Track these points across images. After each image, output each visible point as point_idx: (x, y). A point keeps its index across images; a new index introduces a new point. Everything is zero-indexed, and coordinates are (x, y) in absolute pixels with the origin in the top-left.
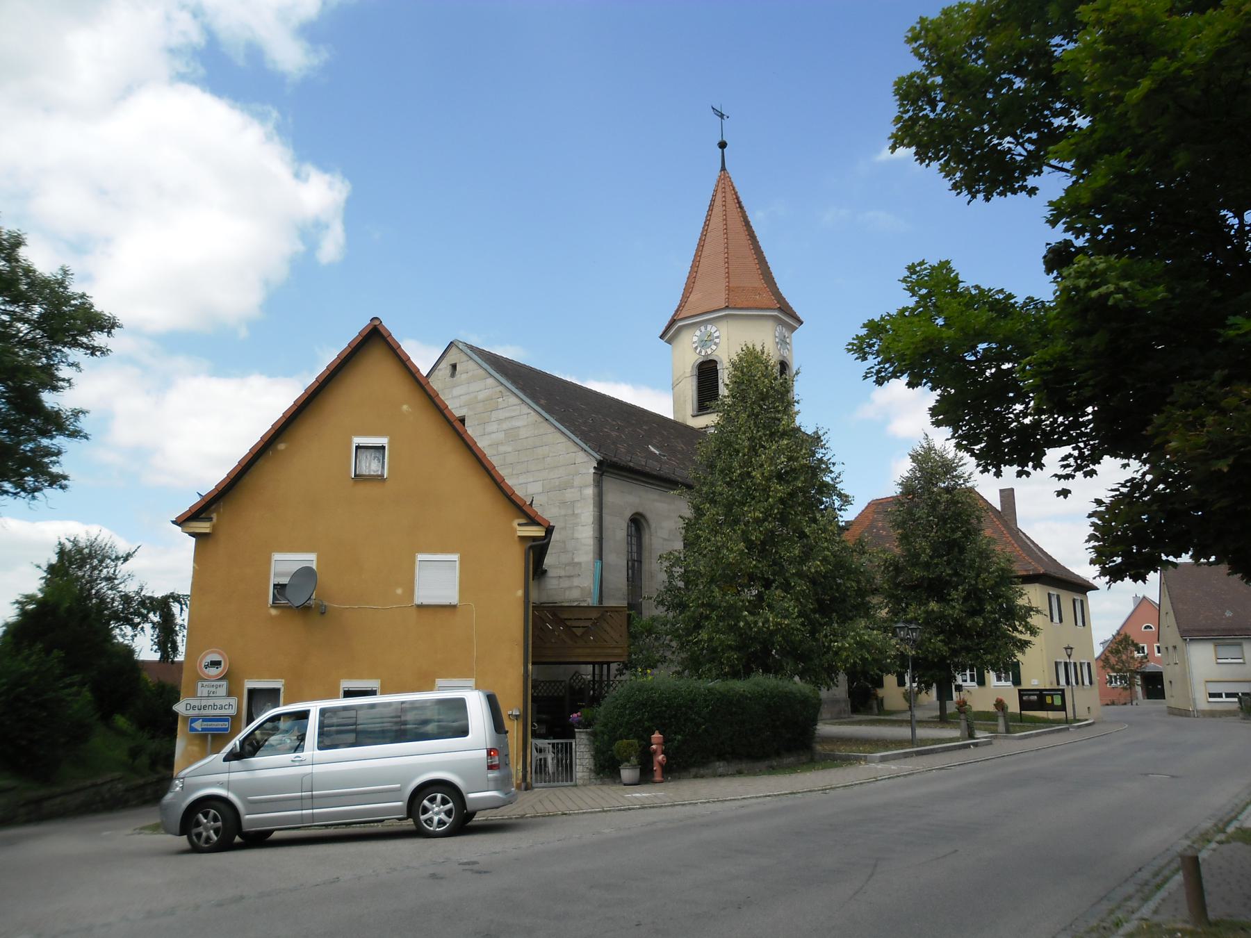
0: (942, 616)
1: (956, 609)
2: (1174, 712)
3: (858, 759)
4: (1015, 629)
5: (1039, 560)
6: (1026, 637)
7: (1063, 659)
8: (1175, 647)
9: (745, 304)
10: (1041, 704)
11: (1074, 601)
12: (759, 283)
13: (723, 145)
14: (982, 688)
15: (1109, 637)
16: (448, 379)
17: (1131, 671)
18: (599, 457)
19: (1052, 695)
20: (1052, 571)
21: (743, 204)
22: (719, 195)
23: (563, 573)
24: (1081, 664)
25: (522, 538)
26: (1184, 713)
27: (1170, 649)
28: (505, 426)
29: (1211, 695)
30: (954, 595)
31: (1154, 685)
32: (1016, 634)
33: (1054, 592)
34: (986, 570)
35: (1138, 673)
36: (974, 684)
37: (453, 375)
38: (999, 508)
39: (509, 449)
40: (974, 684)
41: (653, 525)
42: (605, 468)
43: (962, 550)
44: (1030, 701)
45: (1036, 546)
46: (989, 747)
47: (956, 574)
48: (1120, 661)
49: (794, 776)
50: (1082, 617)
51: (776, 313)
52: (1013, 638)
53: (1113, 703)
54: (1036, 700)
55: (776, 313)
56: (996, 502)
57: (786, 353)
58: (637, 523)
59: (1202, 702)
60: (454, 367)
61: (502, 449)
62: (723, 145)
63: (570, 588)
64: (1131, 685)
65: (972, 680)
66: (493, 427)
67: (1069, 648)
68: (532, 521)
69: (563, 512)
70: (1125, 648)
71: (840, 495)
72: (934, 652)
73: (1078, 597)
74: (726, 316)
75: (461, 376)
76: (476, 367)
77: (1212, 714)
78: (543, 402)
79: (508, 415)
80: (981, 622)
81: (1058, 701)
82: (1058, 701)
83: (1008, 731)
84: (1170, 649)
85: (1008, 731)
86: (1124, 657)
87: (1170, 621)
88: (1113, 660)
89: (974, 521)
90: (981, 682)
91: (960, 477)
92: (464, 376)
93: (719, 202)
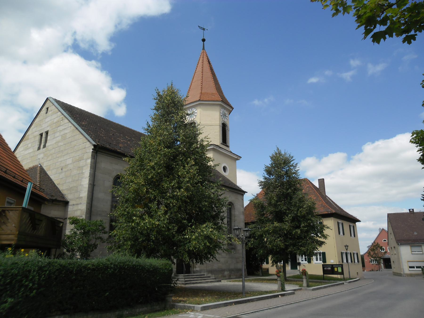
0: (281, 229)
1: (286, 226)
2: (395, 274)
3: (189, 308)
4: (318, 236)
5: (334, 208)
6: (322, 240)
7: (345, 251)
8: (394, 247)
9: (207, 99)
10: (333, 272)
11: (350, 226)
12: (215, 91)
13: (204, 40)
14: (310, 264)
15: (371, 244)
16: (45, 115)
17: (379, 257)
18: (94, 143)
19: (337, 267)
20: (339, 212)
21: (211, 63)
22: (201, 59)
23: (75, 203)
24: (354, 254)
26: (400, 275)
27: (393, 248)
28: (62, 133)
29: (410, 267)
30: (287, 219)
31: (388, 263)
32: (318, 238)
33: (340, 221)
34: (302, 207)
35: (381, 258)
36: (306, 262)
37: (47, 113)
38: (318, 187)
40: (306, 262)
42: (98, 150)
43: (291, 198)
44: (327, 270)
45: (334, 203)
46: (292, 296)
47: (289, 209)
48: (375, 253)
49: (164, 315)
50: (354, 233)
51: (220, 103)
52: (317, 240)
53: (373, 270)
54: (329, 270)
55: (220, 103)
56: (317, 184)
57: (226, 120)
59: (407, 271)
60: (48, 109)
62: (204, 40)
64: (379, 263)
65: (306, 260)
66: (57, 134)
67: (346, 246)
69: (78, 172)
70: (377, 249)
72: (276, 246)
73: (352, 224)
74: (199, 104)
75: (50, 113)
76: (55, 108)
77: (411, 275)
79: (63, 128)
80: (299, 231)
81: (340, 270)
82: (340, 270)
83: (308, 286)
84: (393, 248)
85: (308, 286)
86: (376, 252)
87: (392, 237)
88: (372, 253)
89: (298, 185)
90: (309, 262)
91: (292, 166)
93: (201, 61)
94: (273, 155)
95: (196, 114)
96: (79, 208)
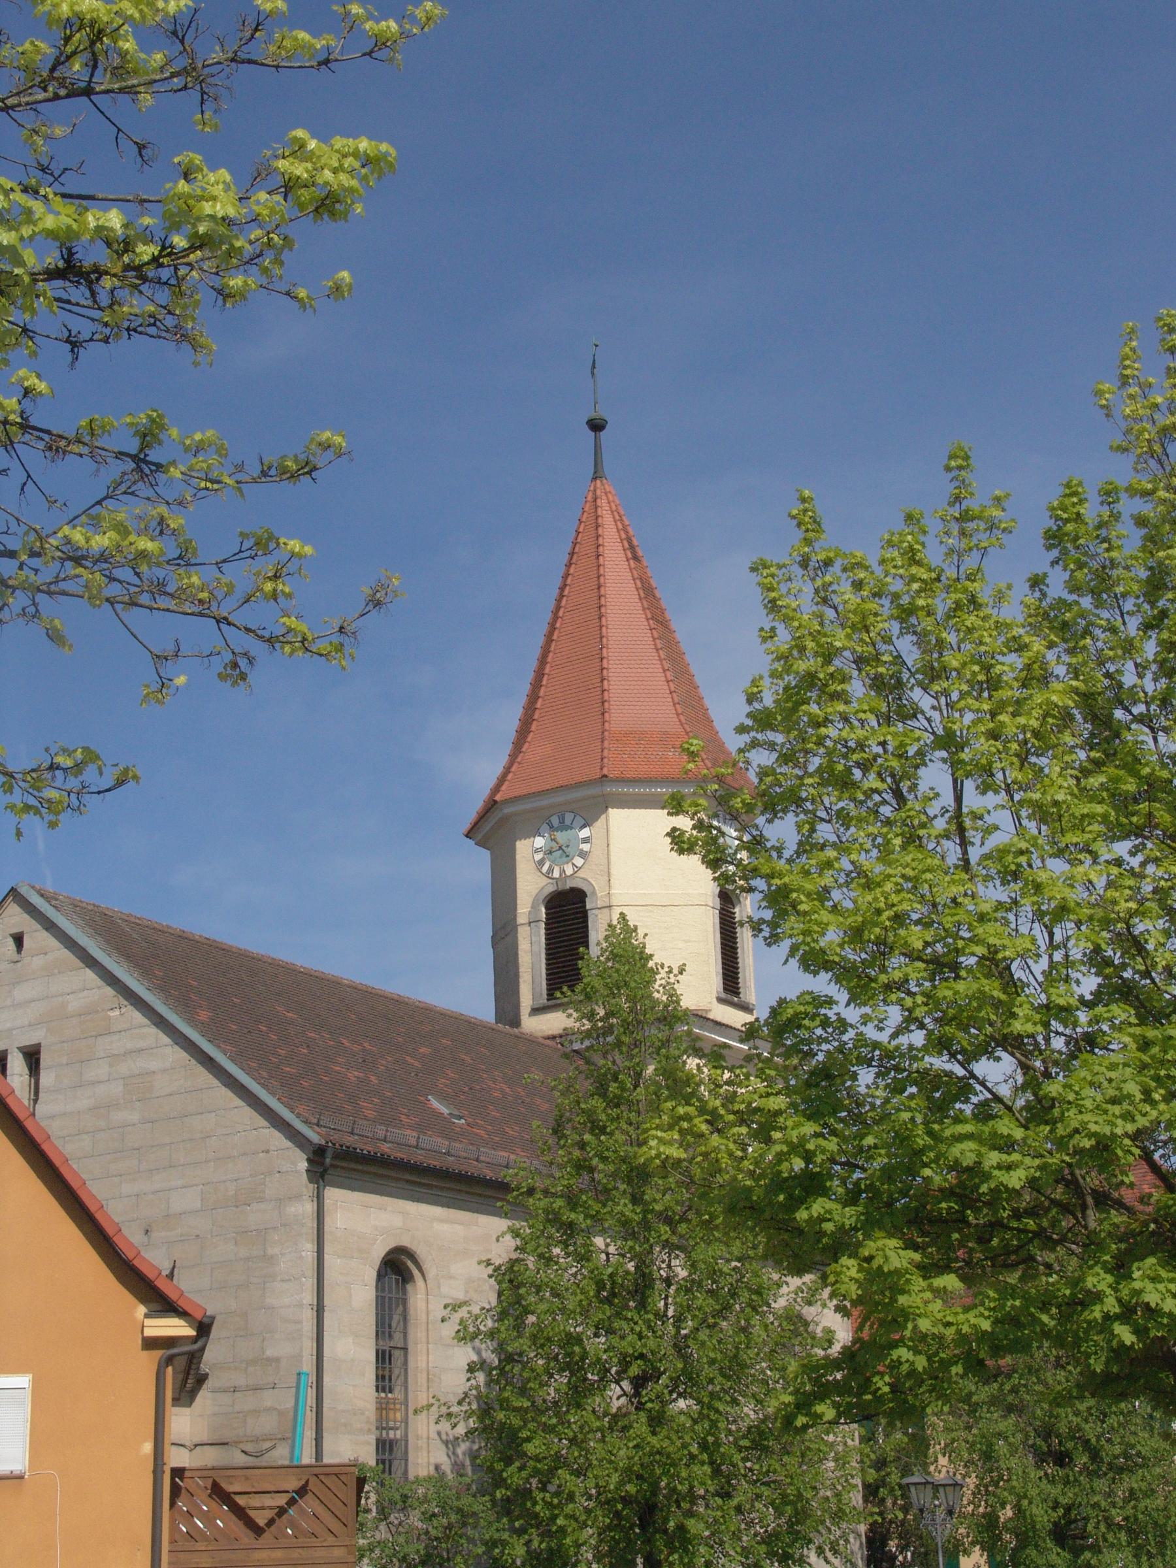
13: (596, 426)
23: (241, 1381)
25: (150, 1344)
39: (135, 1117)
41: (431, 1271)
58: (397, 1268)
61: (118, 1116)
62: (596, 426)
63: (256, 1412)
66: (99, 1070)
68: (165, 1306)
71: (1028, 1037)
78: (204, 1015)
79: (130, 1045)
92: (37, 962)
94: (680, 843)
95: (585, 847)
96: (269, 1404)
